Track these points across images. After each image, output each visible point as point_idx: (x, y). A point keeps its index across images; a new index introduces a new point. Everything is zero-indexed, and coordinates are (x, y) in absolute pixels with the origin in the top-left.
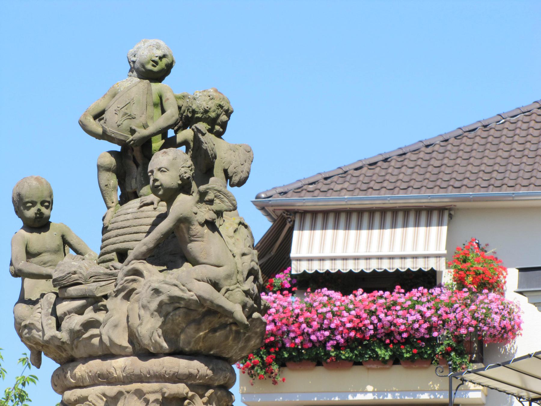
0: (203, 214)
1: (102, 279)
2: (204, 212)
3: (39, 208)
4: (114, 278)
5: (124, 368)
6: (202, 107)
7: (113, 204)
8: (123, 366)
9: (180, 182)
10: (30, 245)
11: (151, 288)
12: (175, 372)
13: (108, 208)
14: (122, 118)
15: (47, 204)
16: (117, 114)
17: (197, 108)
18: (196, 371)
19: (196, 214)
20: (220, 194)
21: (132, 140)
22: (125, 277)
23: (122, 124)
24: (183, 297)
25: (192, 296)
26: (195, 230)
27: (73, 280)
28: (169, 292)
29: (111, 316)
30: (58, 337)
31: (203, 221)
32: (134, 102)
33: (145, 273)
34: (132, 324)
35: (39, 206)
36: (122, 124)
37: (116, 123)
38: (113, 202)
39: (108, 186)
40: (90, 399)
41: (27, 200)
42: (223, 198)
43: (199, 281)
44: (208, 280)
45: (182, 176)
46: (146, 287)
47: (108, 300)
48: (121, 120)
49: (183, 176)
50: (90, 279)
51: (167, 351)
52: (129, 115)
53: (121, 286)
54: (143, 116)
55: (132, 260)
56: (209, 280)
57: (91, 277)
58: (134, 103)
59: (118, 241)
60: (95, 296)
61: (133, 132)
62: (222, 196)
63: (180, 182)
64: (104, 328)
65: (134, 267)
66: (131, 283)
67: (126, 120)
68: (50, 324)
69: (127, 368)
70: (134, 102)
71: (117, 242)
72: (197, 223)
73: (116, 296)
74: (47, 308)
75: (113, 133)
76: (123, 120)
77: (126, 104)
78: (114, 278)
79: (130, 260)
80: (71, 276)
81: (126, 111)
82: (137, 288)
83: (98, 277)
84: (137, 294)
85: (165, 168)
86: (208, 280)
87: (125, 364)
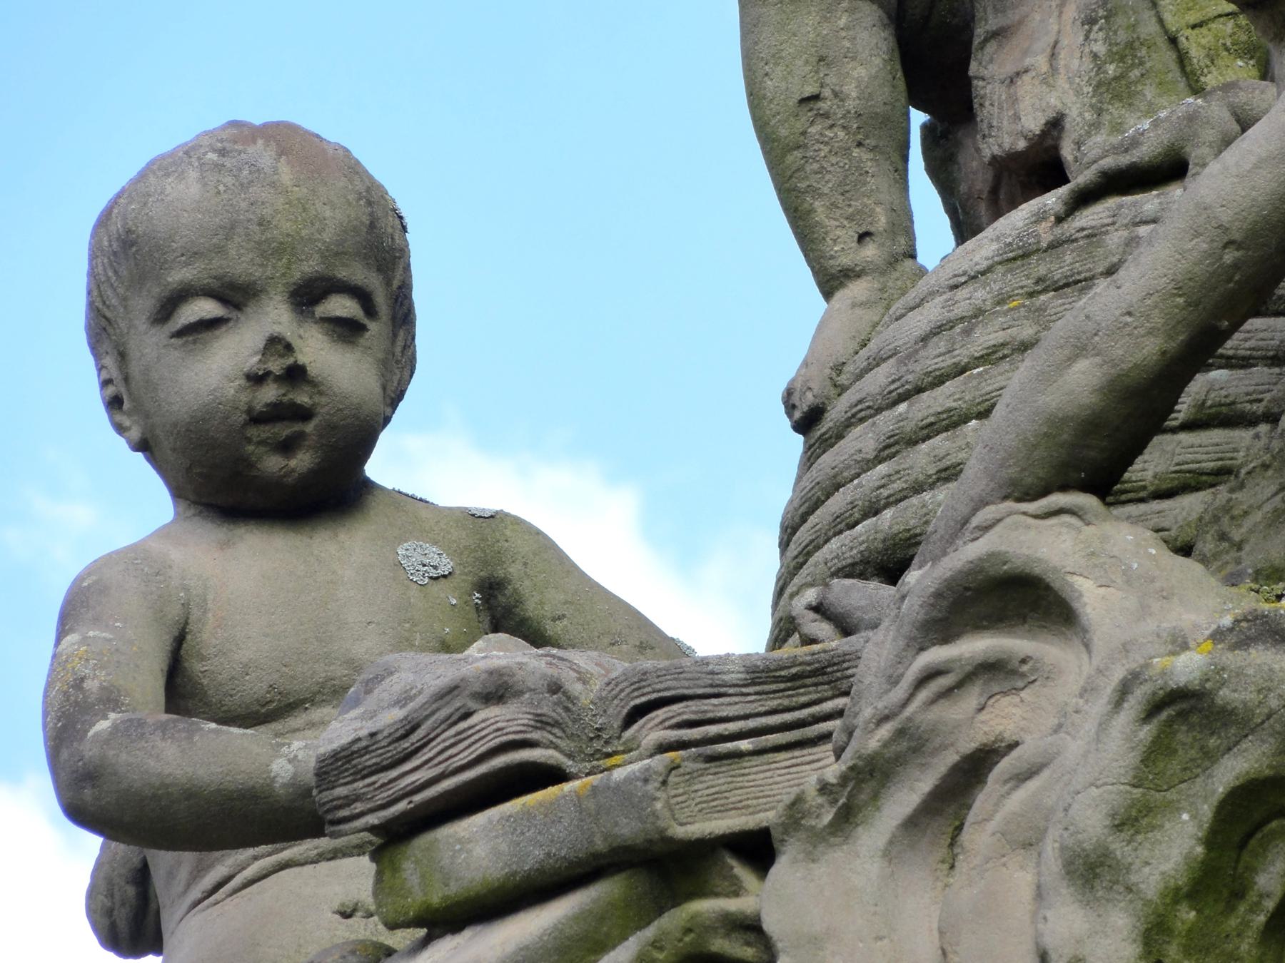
3: (277, 329)
7: (870, 252)
10: (207, 636)
11: (1140, 695)
13: (830, 282)
15: (341, 306)
22: (922, 649)
27: (481, 748)
34: (835, 777)
38: (863, 237)
39: (823, 106)
41: (179, 275)
46: (1100, 705)
47: (774, 871)
50: (628, 734)
53: (885, 731)
55: (983, 503)
60: (670, 840)
65: (991, 555)
66: (971, 698)
71: (885, 492)
73: (847, 818)
80: (467, 715)
83: (693, 705)
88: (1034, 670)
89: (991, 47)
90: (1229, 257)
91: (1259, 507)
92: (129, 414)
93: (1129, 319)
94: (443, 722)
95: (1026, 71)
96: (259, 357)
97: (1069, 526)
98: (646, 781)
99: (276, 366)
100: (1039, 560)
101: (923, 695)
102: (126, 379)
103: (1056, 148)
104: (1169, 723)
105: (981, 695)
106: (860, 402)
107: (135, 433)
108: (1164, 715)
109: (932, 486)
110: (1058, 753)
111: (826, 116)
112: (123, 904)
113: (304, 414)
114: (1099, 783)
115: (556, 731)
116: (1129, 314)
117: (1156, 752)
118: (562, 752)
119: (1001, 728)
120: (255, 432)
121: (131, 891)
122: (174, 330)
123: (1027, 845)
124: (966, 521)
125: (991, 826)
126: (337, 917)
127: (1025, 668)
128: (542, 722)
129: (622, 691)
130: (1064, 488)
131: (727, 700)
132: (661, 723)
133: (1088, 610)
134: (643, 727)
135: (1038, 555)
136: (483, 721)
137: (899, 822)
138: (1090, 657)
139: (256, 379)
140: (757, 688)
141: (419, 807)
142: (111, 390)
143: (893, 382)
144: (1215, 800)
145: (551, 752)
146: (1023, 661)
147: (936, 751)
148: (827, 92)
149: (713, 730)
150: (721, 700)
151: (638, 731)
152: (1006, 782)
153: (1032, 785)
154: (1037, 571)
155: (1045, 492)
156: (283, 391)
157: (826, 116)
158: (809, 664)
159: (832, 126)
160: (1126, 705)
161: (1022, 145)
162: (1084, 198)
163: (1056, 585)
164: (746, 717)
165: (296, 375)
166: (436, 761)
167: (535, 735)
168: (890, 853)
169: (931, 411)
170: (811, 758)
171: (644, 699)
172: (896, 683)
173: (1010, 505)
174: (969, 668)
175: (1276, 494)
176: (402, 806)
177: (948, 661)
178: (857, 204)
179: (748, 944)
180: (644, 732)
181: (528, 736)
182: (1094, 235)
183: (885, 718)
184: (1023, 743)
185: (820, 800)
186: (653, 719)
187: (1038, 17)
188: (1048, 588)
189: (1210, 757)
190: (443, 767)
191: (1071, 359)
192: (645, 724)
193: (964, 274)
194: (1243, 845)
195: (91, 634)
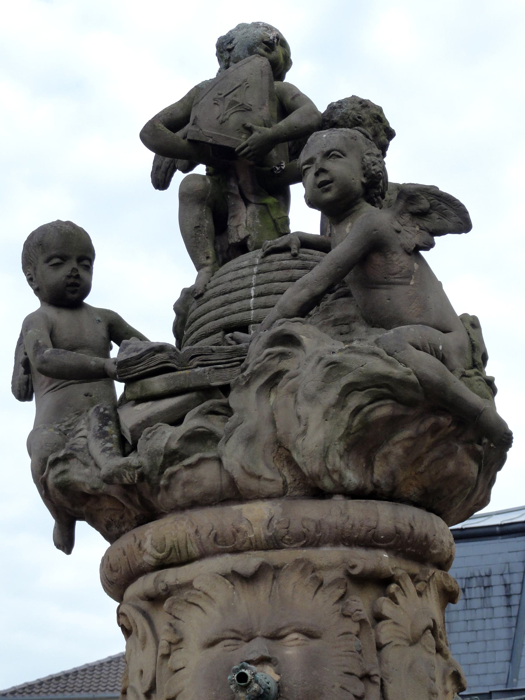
0: (410, 236)
1: (214, 362)
2: (413, 233)
4: (238, 358)
5: (268, 520)
6: (351, 118)
7: (209, 261)
8: (267, 517)
9: (364, 180)
11: (323, 362)
12: (370, 527)
14: (227, 109)
16: (218, 105)
17: (341, 121)
18: (408, 528)
19: (398, 232)
20: (440, 203)
21: (246, 145)
22: (266, 348)
23: (228, 119)
24: (391, 375)
25: (409, 373)
26: (397, 263)
28: (362, 366)
29: (239, 422)
30: (356, 206)
31: (413, 248)
32: (247, 85)
33: (305, 340)
35: (73, 264)
36: (228, 119)
37: (218, 118)
40: (196, 585)
42: (445, 209)
43: (418, 348)
44: (433, 349)
45: (367, 169)
46: (312, 364)
48: (226, 114)
49: (370, 169)
51: (352, 488)
52: (240, 105)
53: (258, 365)
54: (265, 108)
55: (278, 318)
56: (434, 349)
57: (193, 357)
58: (248, 87)
59: (228, 312)
61: (250, 130)
62: (443, 205)
63: (364, 180)
64: (228, 444)
66: (277, 360)
67: (234, 114)
68: (111, 449)
69: (275, 522)
70: (247, 85)
71: (225, 313)
72: (400, 251)
73: (248, 384)
74: (101, 425)
75: (211, 136)
76: (229, 114)
77: (234, 88)
78: (238, 358)
79: (272, 319)
81: (234, 98)
82: (290, 369)
84: (291, 378)
85: (339, 151)
86: (433, 349)
87: (270, 513)
88: (291, 355)
89: (232, 219)
90: (339, 270)
91: (318, 323)
92: (34, 282)
93: (316, 281)
94: (148, 356)
95: (241, 225)
96: (70, 272)
97: (300, 325)
98: (204, 372)
99: (74, 274)
100: (293, 331)
101: (267, 358)
102: (35, 274)
103: (246, 242)
104: (331, 368)
105: (279, 359)
106: (215, 293)
107: (36, 286)
108: (329, 367)
109: (237, 313)
110: (301, 373)
111: (200, 231)
112: (23, 389)
113: (77, 285)
114: (314, 380)
115: (174, 360)
116: (316, 280)
117: (328, 375)
118: (176, 365)
119: (284, 367)
120: (69, 288)
121: (25, 387)
122: (50, 265)
123: (293, 393)
124: (274, 322)
125: (284, 388)
126: (85, 396)
127: (290, 354)
128: (171, 358)
129: (189, 352)
130: (297, 316)
131: (213, 356)
132: (198, 360)
133: (305, 343)
134: (194, 360)
135: (294, 330)
136: (158, 357)
137: (260, 385)
138: (305, 353)
139: (69, 277)
140: (219, 354)
141: (141, 374)
142: (30, 276)
143: (224, 289)
144: (342, 386)
145: (173, 365)
146: (289, 353)
147: (270, 371)
148: (201, 226)
149: (210, 362)
150: (211, 356)
151: (193, 361)
152: (288, 379)
153: (294, 380)
154: (293, 333)
155: (293, 317)
156: (75, 280)
157: (200, 231)
158: (232, 349)
159: (201, 233)
160: (320, 364)
161: (239, 241)
162: (267, 254)
163: (297, 337)
164: (216, 360)
165: (78, 277)
166: (146, 365)
167: (169, 360)
168: (259, 392)
169: (236, 296)
170: (233, 370)
171: (194, 354)
172: (259, 356)
173: (285, 319)
174: (277, 353)
175: (321, 321)
176: (137, 374)
177: (274, 351)
178: (206, 251)
179: (224, 410)
180: (194, 361)
181: (168, 360)
182: (271, 262)
183: (259, 363)
184: (290, 371)
185: (242, 379)
186: (196, 359)
187: (241, 214)
188: (295, 337)
189: (340, 376)
190: (148, 366)
191: (303, 289)
192: (194, 360)
193: (239, 267)
194: (346, 396)
195: (36, 330)
